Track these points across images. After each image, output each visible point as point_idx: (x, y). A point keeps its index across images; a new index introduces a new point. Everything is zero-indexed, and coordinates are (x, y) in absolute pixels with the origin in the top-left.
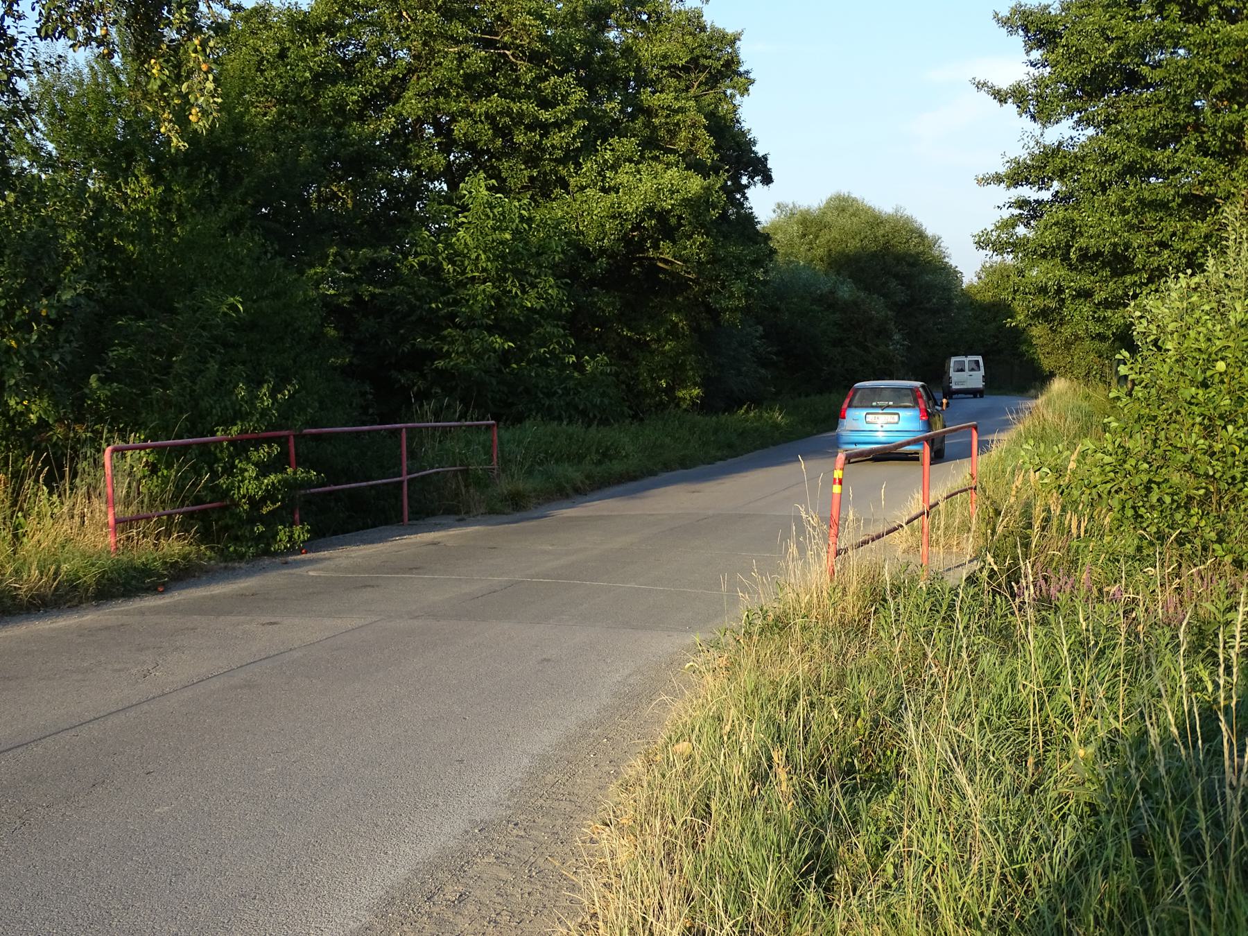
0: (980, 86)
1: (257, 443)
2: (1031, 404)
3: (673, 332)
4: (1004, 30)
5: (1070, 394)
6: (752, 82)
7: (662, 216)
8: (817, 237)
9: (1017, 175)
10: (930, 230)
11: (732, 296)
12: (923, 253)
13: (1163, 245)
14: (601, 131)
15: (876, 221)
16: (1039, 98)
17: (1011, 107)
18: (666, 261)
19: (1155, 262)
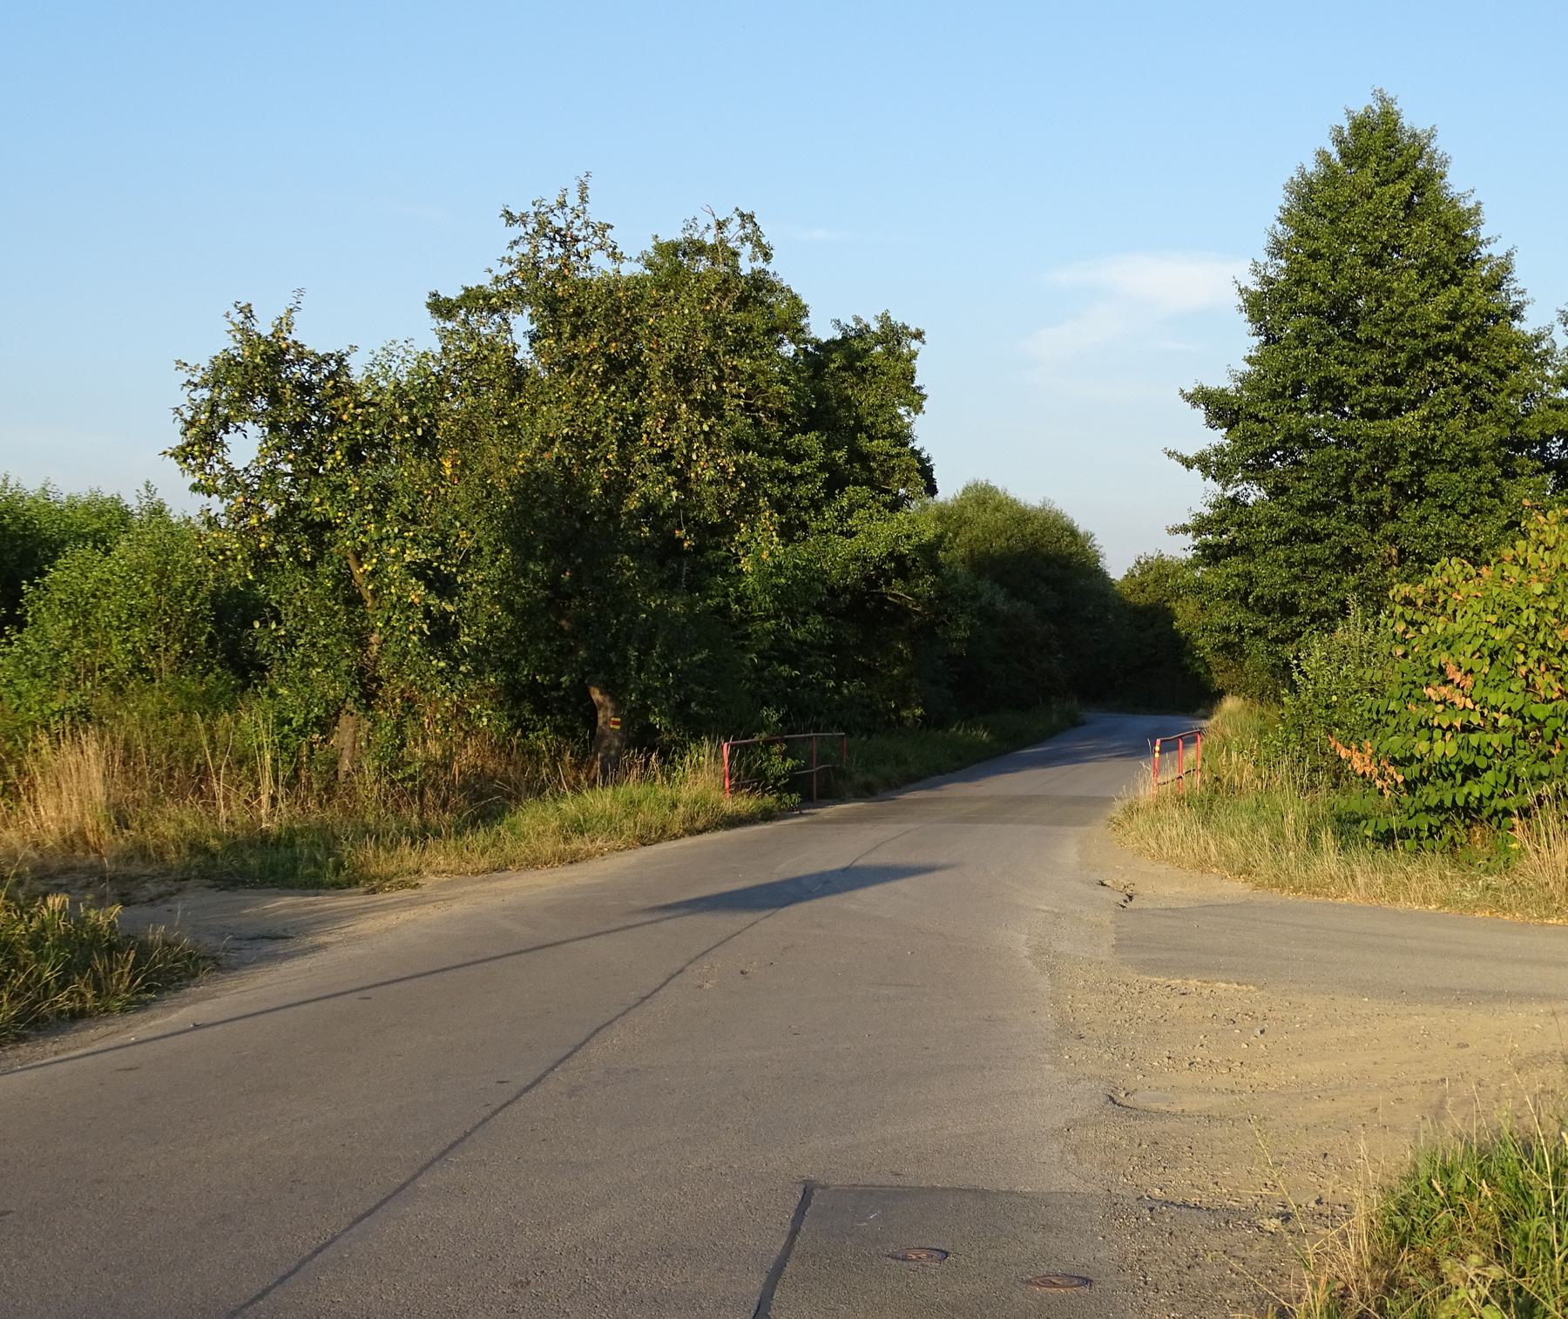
0: (1170, 454)
1: (773, 743)
2: (1205, 724)
3: (900, 659)
4: (1189, 405)
5: (1244, 713)
6: (924, 397)
7: (899, 559)
8: (956, 535)
9: (1202, 525)
10: (1082, 526)
11: (959, 627)
12: (1077, 553)
13: (1322, 593)
14: (836, 481)
15: (1023, 517)
16: (1221, 466)
17: (1196, 472)
18: (895, 596)
19: (1315, 607)
